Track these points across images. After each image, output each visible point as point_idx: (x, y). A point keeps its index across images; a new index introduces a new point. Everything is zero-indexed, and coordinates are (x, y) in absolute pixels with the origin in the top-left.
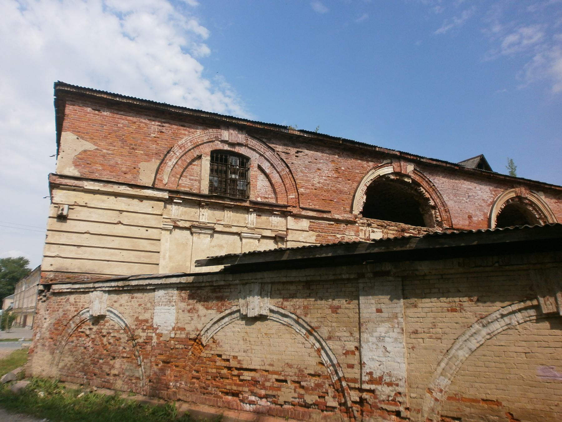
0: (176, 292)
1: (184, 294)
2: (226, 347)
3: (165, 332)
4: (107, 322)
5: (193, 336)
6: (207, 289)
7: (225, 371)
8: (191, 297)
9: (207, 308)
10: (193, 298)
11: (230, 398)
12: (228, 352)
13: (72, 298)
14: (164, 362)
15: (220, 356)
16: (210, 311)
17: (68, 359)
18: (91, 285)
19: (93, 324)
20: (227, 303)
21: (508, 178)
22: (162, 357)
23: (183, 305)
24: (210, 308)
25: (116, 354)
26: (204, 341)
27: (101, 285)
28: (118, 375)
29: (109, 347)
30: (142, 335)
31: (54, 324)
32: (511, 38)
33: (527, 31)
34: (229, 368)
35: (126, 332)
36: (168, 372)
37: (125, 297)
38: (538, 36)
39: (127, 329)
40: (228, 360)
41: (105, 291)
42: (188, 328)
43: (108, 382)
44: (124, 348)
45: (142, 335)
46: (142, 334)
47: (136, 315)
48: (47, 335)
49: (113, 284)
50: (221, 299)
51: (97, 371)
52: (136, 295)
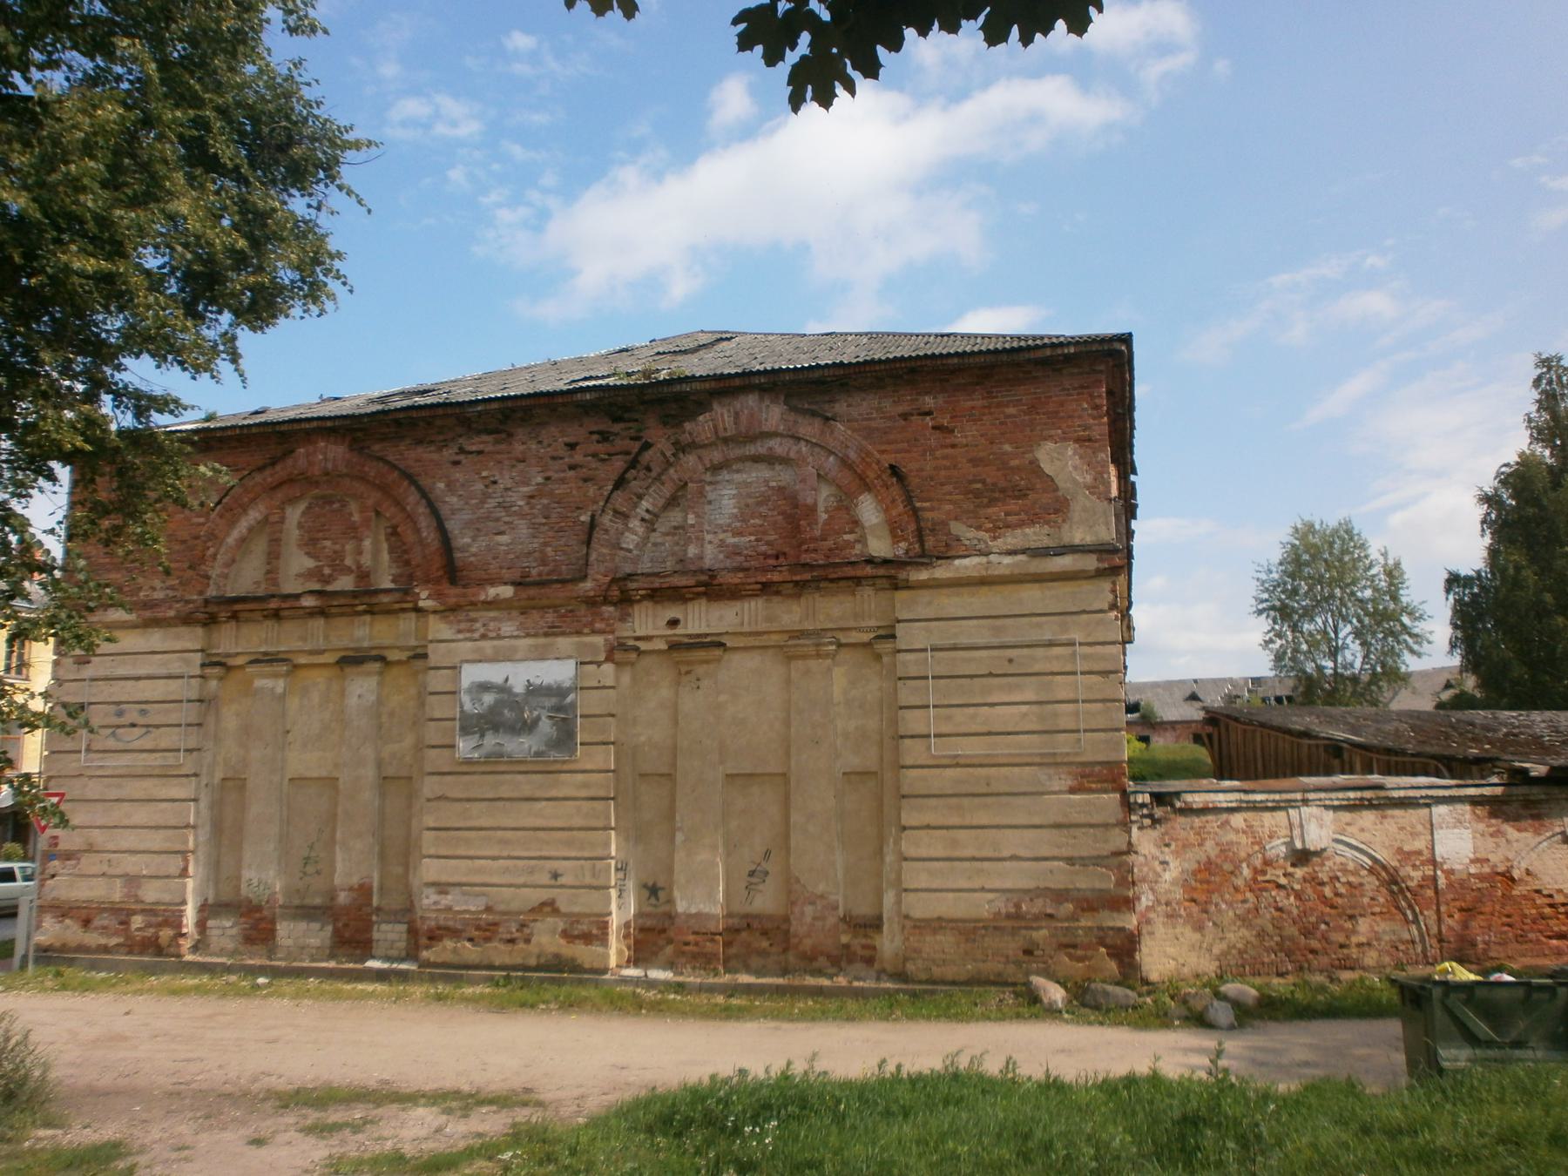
0: (1468, 808)
1: (1479, 811)
2: (1546, 879)
3: (1457, 867)
4: (1328, 859)
5: (1501, 869)
6: (1516, 805)
7: (1547, 910)
8: (1493, 815)
9: (1519, 830)
10: (1496, 817)
11: (1554, 942)
12: (1548, 885)
13: (1238, 820)
14: (1461, 910)
15: (1538, 891)
16: (1524, 834)
17: (1238, 936)
18: (1299, 796)
19: (1293, 865)
20: (1547, 822)
21: (254, 430)
22: (1458, 904)
23: (1481, 826)
24: (1526, 830)
25: (1356, 912)
26: (1516, 874)
27: (1322, 795)
28: (1369, 944)
29: (1340, 901)
30: (1414, 876)
31: (1194, 873)
32: (412, 107)
33: (450, 105)
34: (1551, 906)
35: (1371, 871)
36: (1473, 924)
37: (1368, 818)
38: (470, 129)
39: (1377, 868)
40: (1551, 896)
41: (1326, 807)
42: (1493, 858)
43: (1348, 957)
44: (1372, 899)
45: (1414, 876)
46: (1413, 874)
47: (1397, 844)
48: (1178, 894)
49: (1352, 795)
50: (1537, 817)
51: (1314, 944)
52: (1390, 812)
